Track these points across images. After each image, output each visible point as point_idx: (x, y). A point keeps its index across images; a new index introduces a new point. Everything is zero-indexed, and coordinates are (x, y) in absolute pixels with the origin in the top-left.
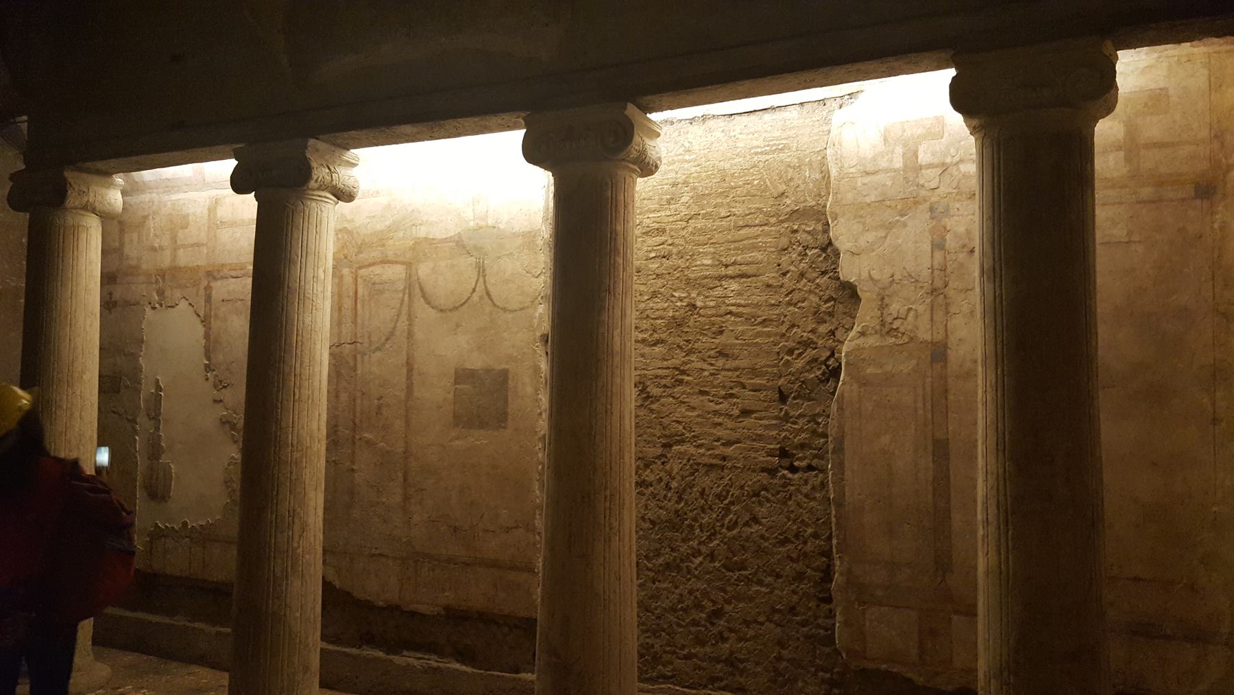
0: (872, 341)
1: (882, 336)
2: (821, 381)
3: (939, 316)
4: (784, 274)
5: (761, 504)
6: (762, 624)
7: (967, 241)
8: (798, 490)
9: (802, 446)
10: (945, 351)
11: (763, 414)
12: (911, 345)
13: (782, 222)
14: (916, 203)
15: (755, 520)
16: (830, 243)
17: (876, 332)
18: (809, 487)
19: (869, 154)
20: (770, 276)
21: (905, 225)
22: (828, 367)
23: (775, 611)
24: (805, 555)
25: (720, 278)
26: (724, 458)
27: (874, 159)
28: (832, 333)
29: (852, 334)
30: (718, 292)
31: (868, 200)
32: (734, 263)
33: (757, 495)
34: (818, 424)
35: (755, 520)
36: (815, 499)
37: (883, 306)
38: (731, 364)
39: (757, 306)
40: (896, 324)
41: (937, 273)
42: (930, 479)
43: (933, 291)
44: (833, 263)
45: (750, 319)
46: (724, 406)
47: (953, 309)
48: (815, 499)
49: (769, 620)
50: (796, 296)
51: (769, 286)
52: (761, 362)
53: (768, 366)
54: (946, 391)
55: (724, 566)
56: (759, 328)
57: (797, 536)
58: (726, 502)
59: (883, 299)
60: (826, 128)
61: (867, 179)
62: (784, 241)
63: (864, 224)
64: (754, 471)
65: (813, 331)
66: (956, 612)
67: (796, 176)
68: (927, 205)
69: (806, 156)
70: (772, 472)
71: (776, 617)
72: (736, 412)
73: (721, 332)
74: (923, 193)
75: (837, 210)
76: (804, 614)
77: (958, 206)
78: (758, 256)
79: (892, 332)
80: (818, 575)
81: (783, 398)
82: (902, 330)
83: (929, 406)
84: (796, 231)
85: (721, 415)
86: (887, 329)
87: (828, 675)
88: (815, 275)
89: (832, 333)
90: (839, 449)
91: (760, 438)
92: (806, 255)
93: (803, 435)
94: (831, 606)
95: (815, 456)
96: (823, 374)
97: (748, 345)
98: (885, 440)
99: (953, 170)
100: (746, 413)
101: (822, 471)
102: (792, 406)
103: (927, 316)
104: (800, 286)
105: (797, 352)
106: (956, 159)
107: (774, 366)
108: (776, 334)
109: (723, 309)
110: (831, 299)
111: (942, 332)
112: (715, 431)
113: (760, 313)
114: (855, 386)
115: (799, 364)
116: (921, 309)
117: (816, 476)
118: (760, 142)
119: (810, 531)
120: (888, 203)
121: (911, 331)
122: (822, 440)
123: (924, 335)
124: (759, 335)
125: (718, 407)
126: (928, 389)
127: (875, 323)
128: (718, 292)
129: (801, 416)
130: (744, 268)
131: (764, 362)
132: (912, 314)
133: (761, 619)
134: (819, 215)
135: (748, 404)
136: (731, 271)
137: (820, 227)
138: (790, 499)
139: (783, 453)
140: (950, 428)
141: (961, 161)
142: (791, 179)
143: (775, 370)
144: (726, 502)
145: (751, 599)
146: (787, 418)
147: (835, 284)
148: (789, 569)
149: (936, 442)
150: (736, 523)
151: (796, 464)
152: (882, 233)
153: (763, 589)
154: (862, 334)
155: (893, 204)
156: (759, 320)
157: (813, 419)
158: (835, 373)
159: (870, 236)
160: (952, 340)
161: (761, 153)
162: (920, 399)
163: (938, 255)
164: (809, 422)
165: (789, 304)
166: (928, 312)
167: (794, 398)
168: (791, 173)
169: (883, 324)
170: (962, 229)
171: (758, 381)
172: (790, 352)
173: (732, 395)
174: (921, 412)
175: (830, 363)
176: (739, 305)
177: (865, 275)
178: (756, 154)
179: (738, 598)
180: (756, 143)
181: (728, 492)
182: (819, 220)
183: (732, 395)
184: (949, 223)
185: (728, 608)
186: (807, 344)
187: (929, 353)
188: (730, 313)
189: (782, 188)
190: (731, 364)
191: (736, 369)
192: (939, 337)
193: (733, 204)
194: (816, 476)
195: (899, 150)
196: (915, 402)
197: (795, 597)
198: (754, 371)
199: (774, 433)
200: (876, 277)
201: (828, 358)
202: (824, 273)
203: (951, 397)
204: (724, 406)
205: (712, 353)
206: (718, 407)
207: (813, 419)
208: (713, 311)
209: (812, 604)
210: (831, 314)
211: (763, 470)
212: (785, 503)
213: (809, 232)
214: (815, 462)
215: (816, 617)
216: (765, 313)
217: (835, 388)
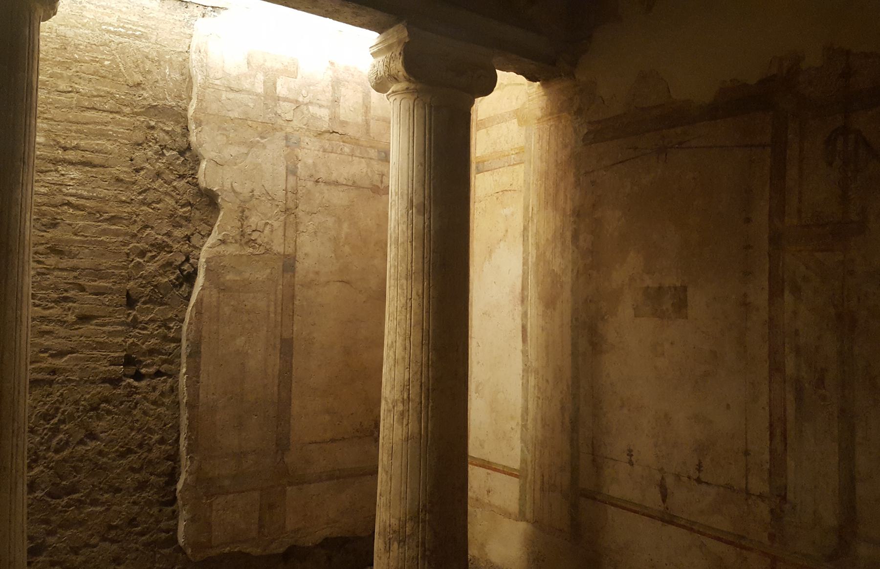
0: (231, 249)
1: (241, 245)
2: (175, 286)
3: (290, 232)
4: (137, 171)
5: (99, 418)
6: (95, 546)
7: (314, 172)
8: (145, 398)
9: (151, 352)
11: (107, 320)
13: (138, 114)
14: (275, 129)
15: (92, 436)
16: (189, 148)
17: (236, 242)
18: (157, 393)
19: (234, 72)
20: (121, 170)
21: (264, 147)
22: (182, 271)
23: (111, 528)
24: (150, 462)
25: (56, 162)
26: (54, 372)
27: (238, 78)
28: (188, 238)
29: (211, 241)
30: (52, 177)
31: (232, 115)
32: (76, 148)
33: (95, 408)
34: (169, 328)
35: (92, 436)
36: (163, 404)
37: (243, 218)
38: (66, 263)
39: (103, 200)
41: (289, 194)
43: (287, 210)
44: (192, 169)
45: (92, 214)
46: (56, 311)
47: (301, 228)
48: (163, 404)
49: (104, 539)
50: (151, 196)
51: (118, 180)
52: (106, 263)
53: (115, 267)
55: (49, 494)
56: (105, 226)
57: (140, 446)
58: (56, 420)
59: (243, 211)
60: (188, 32)
61: (232, 95)
62: (139, 136)
64: (93, 382)
65: (168, 234)
66: (290, 484)
67: (155, 70)
68: (283, 134)
69: (167, 53)
70: (115, 382)
71: (112, 534)
72: (71, 318)
73: (55, 225)
74: (280, 121)
75: (201, 116)
76: (145, 522)
77: (307, 140)
78: (109, 146)
79: (251, 242)
80: (163, 480)
81: (131, 301)
82: (259, 241)
84: (153, 128)
85: (50, 321)
86: (245, 239)
88: (172, 177)
89: (188, 238)
90: (195, 354)
91: (102, 346)
92: (163, 154)
93: (153, 341)
94: (174, 507)
95: (164, 362)
96: (177, 279)
97: (90, 243)
98: (240, 341)
99: (304, 108)
100: (84, 319)
101: (170, 376)
102: (141, 311)
103: (280, 233)
104: (156, 185)
105: (150, 254)
106: (306, 100)
107: (122, 268)
108: (126, 234)
109: (59, 198)
111: (292, 246)
112: (41, 340)
113: (107, 209)
114: (214, 292)
115: (152, 267)
116: (276, 224)
117: (165, 381)
118: (113, 20)
119: (156, 437)
120: (250, 123)
121: (267, 243)
122: (173, 345)
123: (278, 247)
124: (104, 232)
125: (47, 312)
127: (235, 232)
128: (52, 177)
129: (152, 320)
130: (88, 156)
131: (110, 263)
133: (93, 541)
134: (180, 116)
135: (86, 309)
136: (71, 155)
137: (178, 130)
138: (135, 407)
139: (129, 361)
140: (295, 329)
141: (311, 103)
142: (149, 72)
143: (124, 272)
144: (56, 420)
145: (81, 523)
146: (135, 324)
147: (192, 190)
148: (130, 480)
149: (283, 341)
150: (67, 443)
151: (143, 371)
152: (244, 150)
153: (98, 509)
154: (223, 242)
155: (254, 125)
156: (106, 216)
157: (165, 324)
158: (190, 278)
159: (234, 150)
160: (300, 255)
161: (115, 33)
163: (291, 179)
164: (160, 327)
165: (143, 203)
166: (282, 228)
167: (145, 303)
168: (148, 66)
169: (243, 235)
170: (310, 161)
171: (102, 283)
172: (142, 254)
173: (66, 299)
174: (272, 315)
176: (81, 197)
177: (227, 186)
178: (108, 31)
179: (66, 525)
180: (107, 19)
181: (57, 409)
182: (178, 122)
183: (66, 299)
184: (301, 154)
185: (51, 540)
186: (161, 247)
188: (69, 204)
189: (138, 78)
190: (66, 263)
191: (74, 269)
192: (290, 251)
193: (76, 80)
194: (165, 381)
195: (260, 77)
196: (268, 306)
197: (136, 508)
198: (97, 273)
199: (120, 340)
201: (183, 264)
202: (182, 177)
203: (297, 302)
204: (56, 311)
205: (41, 248)
206: (47, 312)
207: (165, 324)
208: (45, 199)
209: (155, 510)
210: (188, 219)
211: (104, 381)
212: (129, 413)
213: (167, 132)
214: (164, 368)
215: (158, 522)
216: (114, 210)
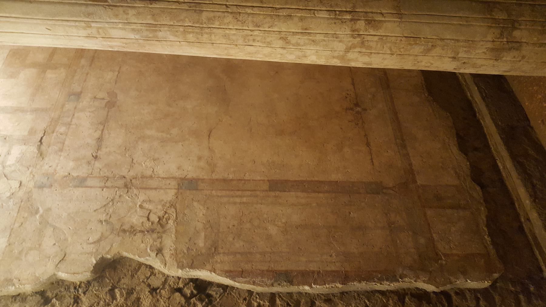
0: (169, 242)
1: (164, 232)
3: (153, 183)
10: (187, 179)
12: (178, 206)
16: (42, 293)
22: (193, 295)
28: (153, 290)
29: (157, 265)
37: (133, 231)
40: (154, 218)
42: (305, 195)
43: (126, 186)
47: (149, 173)
54: (225, 180)
59: (124, 231)
63: (31, 249)
74: (21, 194)
79: (162, 222)
83: (239, 193)
87: (521, 297)
89: (153, 290)
96: (201, 300)
110: (112, 292)
111: (168, 182)
114: (218, 258)
116: (142, 197)
120: (17, 225)
121: (164, 206)
122: (278, 301)
126: (224, 193)
127: (149, 239)
132: (146, 205)
140: (259, 178)
147: (94, 288)
149: (271, 189)
154: (159, 251)
162: (231, 199)
170: (71, 164)
174: (244, 200)
175: (188, 292)
177: (91, 248)
184: (61, 173)
187: (188, 192)
192: (174, 183)
196: (235, 203)
200: (96, 237)
201: (184, 295)
203: (231, 177)
210: (130, 292)
217: (219, 285)
